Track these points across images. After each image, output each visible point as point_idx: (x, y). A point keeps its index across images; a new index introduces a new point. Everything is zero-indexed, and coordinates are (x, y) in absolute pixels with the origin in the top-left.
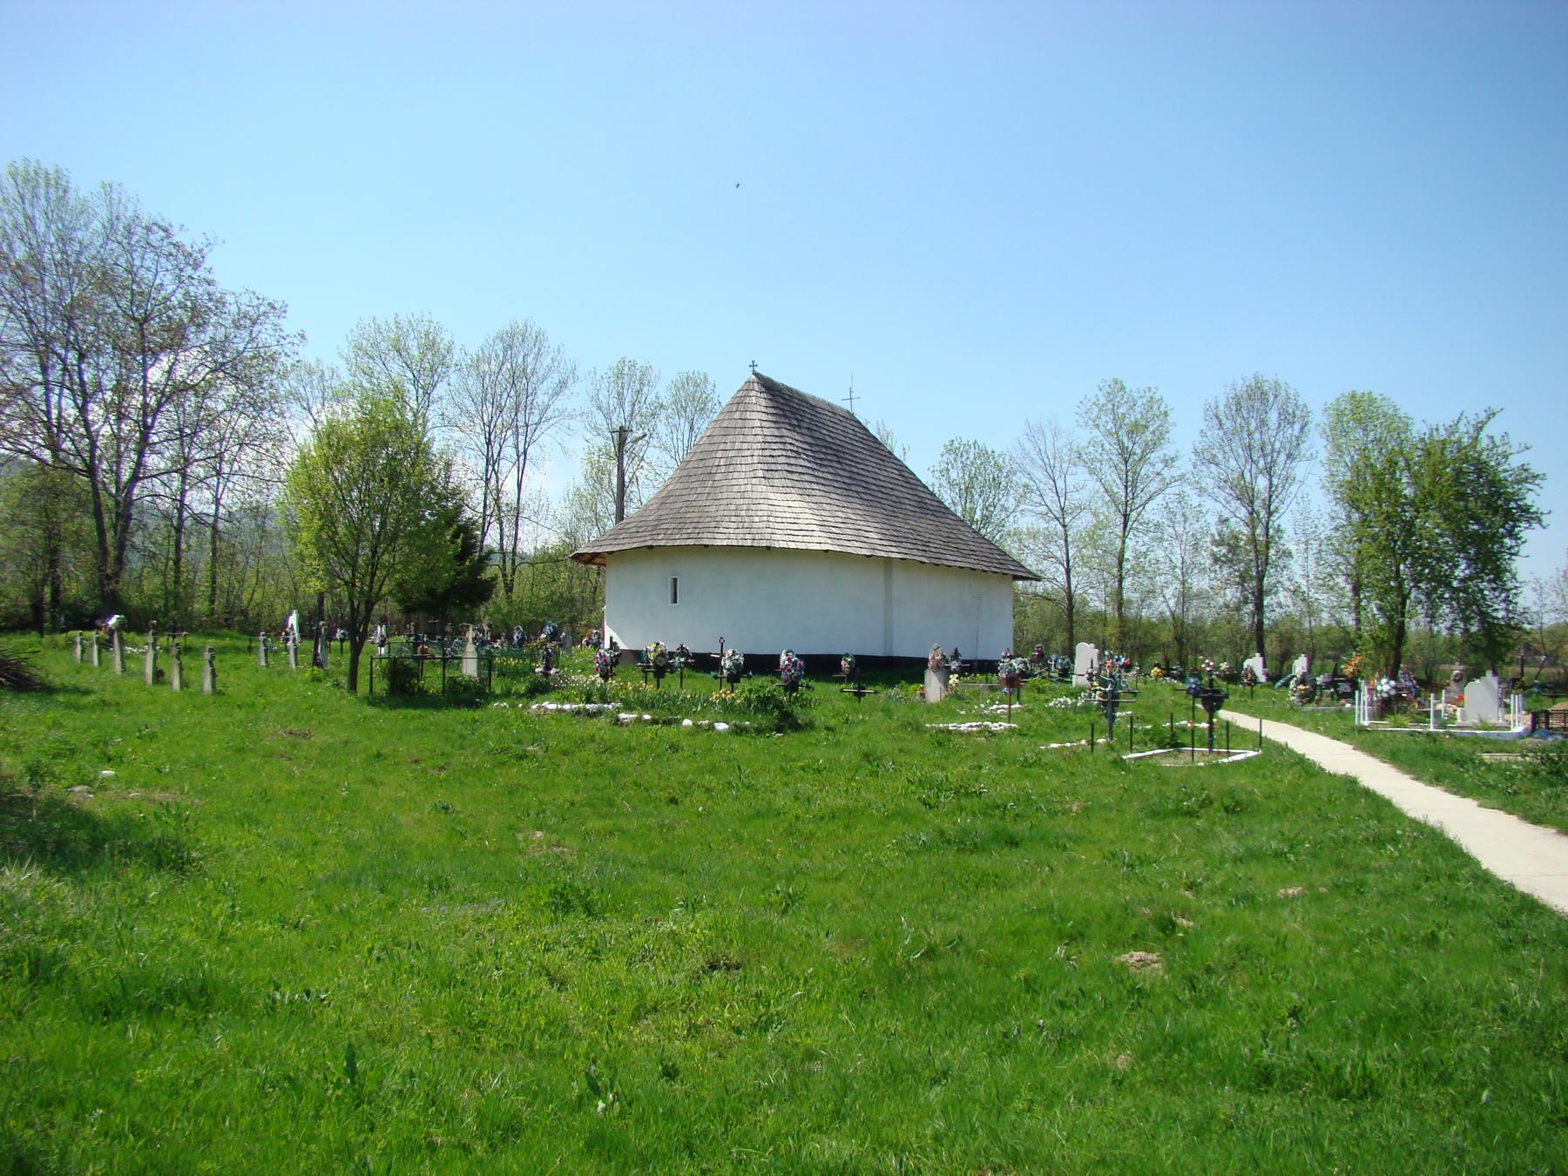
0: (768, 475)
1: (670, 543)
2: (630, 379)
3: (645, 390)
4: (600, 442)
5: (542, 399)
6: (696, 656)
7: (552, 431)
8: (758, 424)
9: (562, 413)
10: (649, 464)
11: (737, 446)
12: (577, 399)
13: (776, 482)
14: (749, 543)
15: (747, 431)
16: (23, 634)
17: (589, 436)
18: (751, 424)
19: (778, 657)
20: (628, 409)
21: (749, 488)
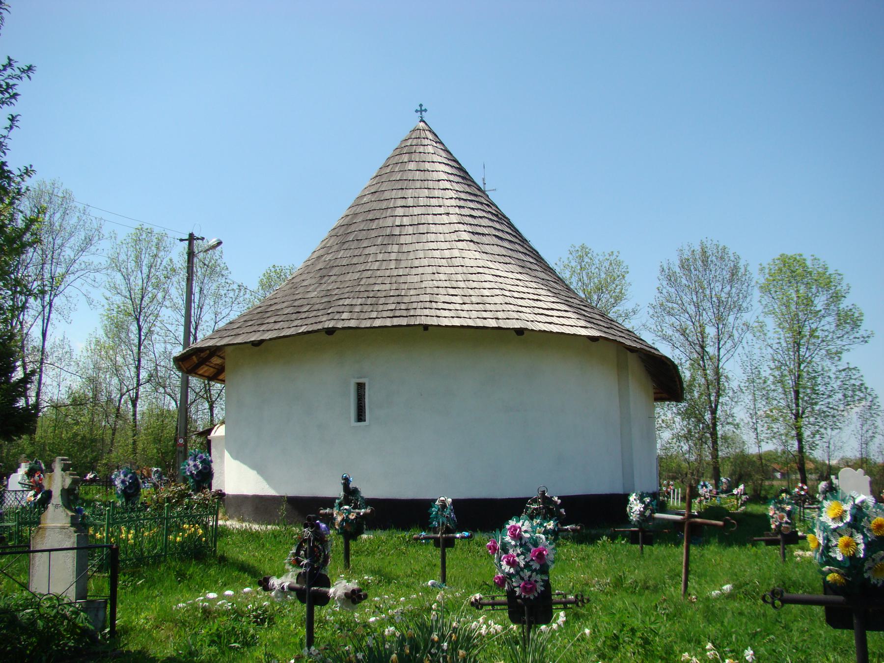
0: (475, 238)
1: (367, 324)
2: (145, 242)
3: (161, 254)
4: (118, 300)
5: (68, 253)
6: (568, 501)
7: (78, 283)
8: (444, 176)
9: (88, 266)
10: (162, 322)
11: (422, 202)
12: (99, 255)
13: (488, 249)
14: (493, 323)
15: (431, 184)
16: (755, 512)
17: (108, 294)
18: (435, 176)
19: (623, 500)
20: (145, 270)
21: (456, 253)
